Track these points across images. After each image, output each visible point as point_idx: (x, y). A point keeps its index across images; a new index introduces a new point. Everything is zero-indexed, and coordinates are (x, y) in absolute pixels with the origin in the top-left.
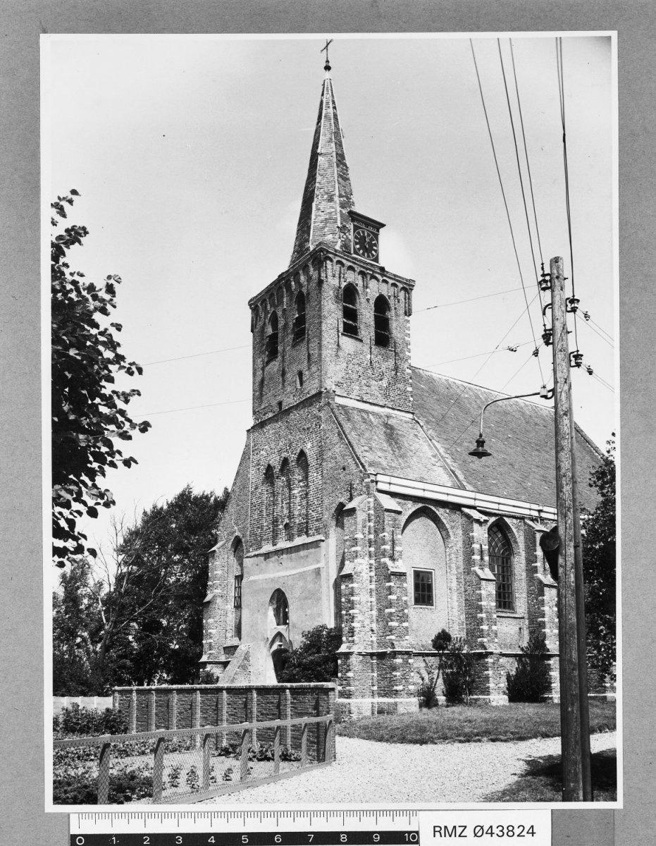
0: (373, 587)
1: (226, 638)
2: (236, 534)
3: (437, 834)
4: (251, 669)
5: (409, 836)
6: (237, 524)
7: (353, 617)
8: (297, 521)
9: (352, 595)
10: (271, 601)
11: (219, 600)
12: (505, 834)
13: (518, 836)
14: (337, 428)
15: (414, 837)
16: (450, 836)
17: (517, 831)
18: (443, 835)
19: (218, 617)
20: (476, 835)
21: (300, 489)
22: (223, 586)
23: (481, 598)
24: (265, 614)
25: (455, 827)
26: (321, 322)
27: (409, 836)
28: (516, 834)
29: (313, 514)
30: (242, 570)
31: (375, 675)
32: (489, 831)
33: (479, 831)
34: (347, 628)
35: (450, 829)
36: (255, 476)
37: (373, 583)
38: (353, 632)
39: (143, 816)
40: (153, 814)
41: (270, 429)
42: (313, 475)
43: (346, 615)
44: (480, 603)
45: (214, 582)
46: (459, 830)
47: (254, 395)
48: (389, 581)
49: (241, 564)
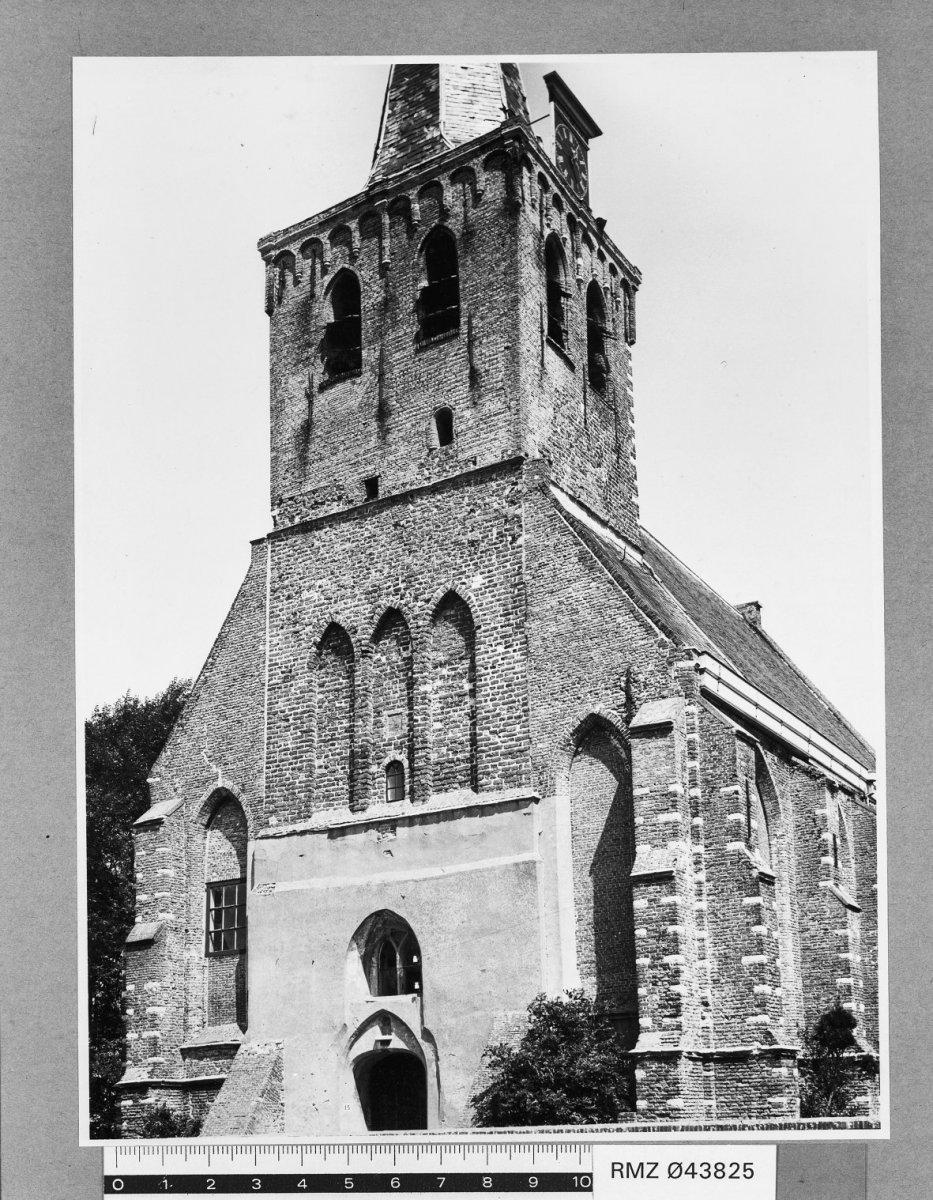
0: (704, 905)
1: (187, 1028)
2: (220, 784)
3: (617, 1174)
4: (285, 1098)
5: (579, 1180)
6: (220, 761)
7: (678, 972)
8: (434, 757)
9: (674, 922)
10: (355, 938)
11: (170, 938)
12: (712, 1174)
13: (731, 1177)
14: (577, 544)
15: (586, 1182)
16: (635, 1176)
17: (729, 1171)
18: (625, 1174)
19: (168, 979)
20: (671, 1176)
21: (439, 683)
22: (178, 906)
23: (846, 945)
24: (337, 971)
25: (641, 1164)
26: (516, 301)
27: (579, 1180)
28: (728, 1175)
29: (495, 739)
30: (243, 867)
31: (713, 1103)
32: (690, 1171)
33: (676, 1171)
34: (656, 997)
35: (635, 1167)
36: (280, 647)
37: (704, 897)
38: (678, 1007)
39: (207, 1150)
40: (220, 1148)
41: (334, 541)
42: (490, 650)
43: (652, 967)
44: (843, 956)
45: (157, 895)
46: (647, 1169)
47: (274, 460)
48: (757, 894)
49: (242, 854)
